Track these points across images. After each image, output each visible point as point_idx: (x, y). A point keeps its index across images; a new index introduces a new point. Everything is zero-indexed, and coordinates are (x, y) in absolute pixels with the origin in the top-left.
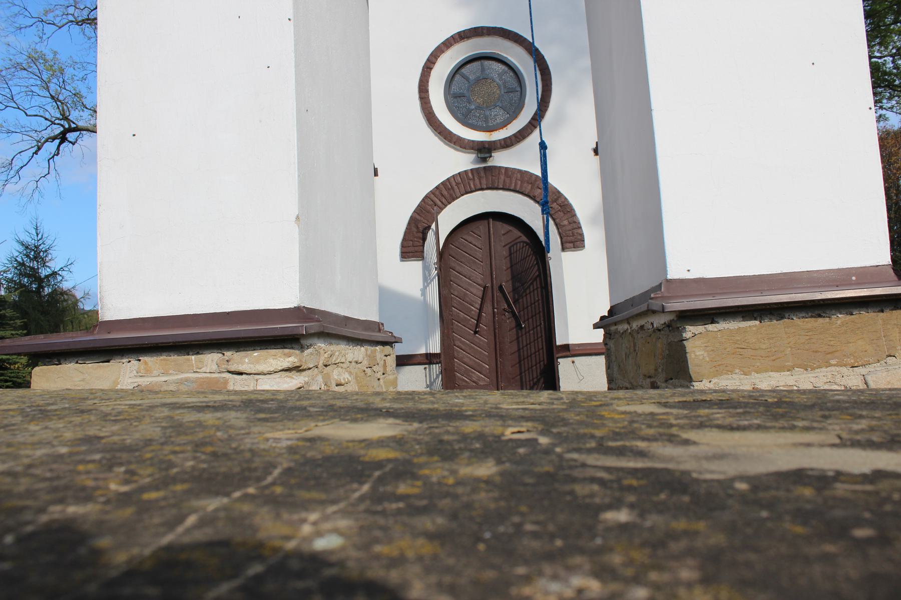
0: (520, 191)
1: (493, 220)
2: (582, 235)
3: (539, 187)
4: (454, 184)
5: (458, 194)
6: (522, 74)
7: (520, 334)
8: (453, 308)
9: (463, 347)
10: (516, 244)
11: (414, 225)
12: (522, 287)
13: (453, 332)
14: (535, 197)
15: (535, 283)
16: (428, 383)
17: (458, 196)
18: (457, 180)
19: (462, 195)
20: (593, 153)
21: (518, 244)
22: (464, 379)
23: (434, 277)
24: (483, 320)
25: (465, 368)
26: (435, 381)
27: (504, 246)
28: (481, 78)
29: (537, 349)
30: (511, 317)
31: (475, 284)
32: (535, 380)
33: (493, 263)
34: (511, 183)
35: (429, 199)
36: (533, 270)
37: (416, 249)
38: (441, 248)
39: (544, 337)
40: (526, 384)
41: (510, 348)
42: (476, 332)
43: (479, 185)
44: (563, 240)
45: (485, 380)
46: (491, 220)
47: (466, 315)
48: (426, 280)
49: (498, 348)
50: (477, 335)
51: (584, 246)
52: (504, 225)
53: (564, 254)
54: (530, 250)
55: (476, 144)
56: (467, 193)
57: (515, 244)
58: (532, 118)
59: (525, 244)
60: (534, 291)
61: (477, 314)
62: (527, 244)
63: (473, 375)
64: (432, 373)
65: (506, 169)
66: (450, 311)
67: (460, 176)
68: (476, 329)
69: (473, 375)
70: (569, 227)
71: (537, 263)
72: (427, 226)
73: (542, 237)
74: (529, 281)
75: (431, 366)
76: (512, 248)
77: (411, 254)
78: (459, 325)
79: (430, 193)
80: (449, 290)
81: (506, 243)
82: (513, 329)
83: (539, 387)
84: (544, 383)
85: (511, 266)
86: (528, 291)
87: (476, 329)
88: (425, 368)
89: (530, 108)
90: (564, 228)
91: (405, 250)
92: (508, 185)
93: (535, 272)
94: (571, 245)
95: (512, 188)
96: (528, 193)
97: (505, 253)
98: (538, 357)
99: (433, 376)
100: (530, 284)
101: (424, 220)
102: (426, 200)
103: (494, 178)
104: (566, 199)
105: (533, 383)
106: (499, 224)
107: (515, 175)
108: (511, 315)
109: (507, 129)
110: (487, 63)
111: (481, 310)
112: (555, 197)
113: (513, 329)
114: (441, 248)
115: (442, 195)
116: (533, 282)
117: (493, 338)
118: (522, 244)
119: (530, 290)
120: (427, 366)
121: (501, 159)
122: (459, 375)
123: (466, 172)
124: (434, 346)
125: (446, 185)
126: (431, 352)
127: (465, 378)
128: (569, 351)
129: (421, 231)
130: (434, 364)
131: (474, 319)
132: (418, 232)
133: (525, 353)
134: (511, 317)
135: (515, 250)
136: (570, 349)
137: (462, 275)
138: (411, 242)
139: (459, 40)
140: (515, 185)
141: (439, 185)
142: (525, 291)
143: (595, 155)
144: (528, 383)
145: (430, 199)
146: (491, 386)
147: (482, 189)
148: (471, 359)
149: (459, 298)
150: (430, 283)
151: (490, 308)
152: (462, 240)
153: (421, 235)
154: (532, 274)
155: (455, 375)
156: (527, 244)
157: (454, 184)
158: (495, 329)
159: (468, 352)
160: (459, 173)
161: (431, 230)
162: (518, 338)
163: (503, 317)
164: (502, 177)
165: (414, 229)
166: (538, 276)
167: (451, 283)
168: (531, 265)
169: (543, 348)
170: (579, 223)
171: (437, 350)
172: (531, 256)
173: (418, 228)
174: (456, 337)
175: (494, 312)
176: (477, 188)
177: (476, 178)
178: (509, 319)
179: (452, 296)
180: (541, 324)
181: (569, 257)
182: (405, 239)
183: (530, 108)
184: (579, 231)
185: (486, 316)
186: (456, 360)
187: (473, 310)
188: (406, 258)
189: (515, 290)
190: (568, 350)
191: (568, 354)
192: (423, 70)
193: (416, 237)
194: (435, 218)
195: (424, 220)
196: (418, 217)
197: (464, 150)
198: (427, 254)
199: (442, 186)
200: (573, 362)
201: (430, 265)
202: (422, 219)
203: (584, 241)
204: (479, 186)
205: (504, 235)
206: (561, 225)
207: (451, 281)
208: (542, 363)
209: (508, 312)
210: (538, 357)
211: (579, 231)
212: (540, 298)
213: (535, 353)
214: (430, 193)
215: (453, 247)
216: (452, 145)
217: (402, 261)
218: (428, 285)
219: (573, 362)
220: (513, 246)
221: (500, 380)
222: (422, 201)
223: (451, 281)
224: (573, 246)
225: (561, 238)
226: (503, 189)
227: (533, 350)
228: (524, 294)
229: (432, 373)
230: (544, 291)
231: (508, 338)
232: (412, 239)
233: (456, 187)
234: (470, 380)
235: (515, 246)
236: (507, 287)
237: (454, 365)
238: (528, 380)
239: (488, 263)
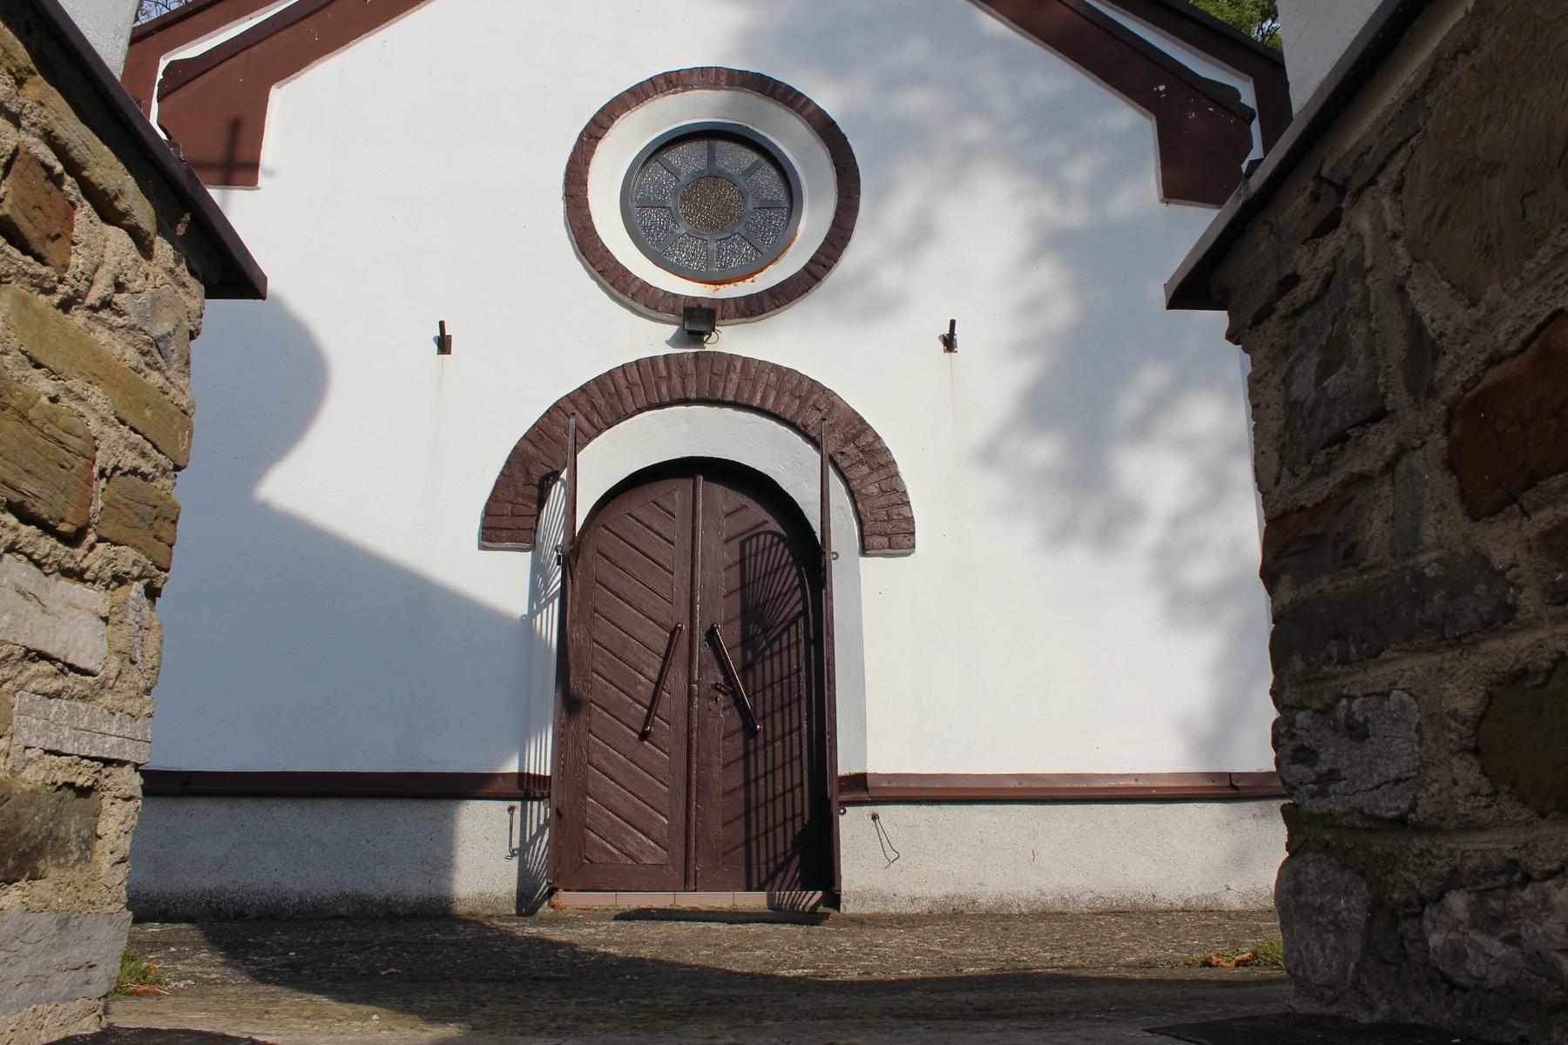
0: (772, 411)
1: (704, 480)
2: (910, 520)
3: (817, 405)
4: (622, 383)
5: (631, 408)
6: (796, 172)
7: (752, 747)
8: (595, 675)
9: (610, 770)
10: (757, 535)
11: (519, 466)
12: (762, 636)
13: (590, 731)
14: (806, 427)
15: (793, 628)
16: (516, 845)
17: (629, 411)
18: (632, 377)
19: (640, 411)
20: (941, 346)
21: (762, 537)
22: (606, 848)
23: (554, 597)
24: (663, 708)
25: (612, 820)
26: (534, 839)
27: (727, 541)
28: (706, 174)
29: (788, 786)
30: (730, 707)
31: (651, 623)
32: (779, 861)
33: (698, 576)
34: (753, 393)
35: (561, 413)
36: (788, 601)
37: (519, 522)
38: (577, 532)
39: (805, 758)
40: (759, 869)
41: (723, 778)
42: (644, 736)
43: (681, 392)
44: (865, 528)
45: (656, 854)
46: (702, 478)
47: (623, 691)
48: (536, 595)
49: (694, 778)
50: (646, 743)
51: (914, 546)
52: (731, 492)
53: (863, 560)
54: (787, 552)
55: (681, 303)
56: (651, 407)
57: (753, 536)
58: (811, 260)
59: (776, 540)
60: (789, 647)
61: (650, 694)
62: (782, 539)
63: (628, 839)
64: (528, 823)
65: (745, 360)
66: (587, 681)
67: (638, 370)
68: (646, 725)
69: (628, 839)
70: (883, 501)
71: (801, 585)
72: (550, 471)
73: (816, 525)
74: (778, 626)
75: (529, 803)
76: (748, 544)
77: (505, 534)
78: (606, 715)
79: (567, 399)
80: (589, 633)
81: (731, 534)
82: (734, 733)
83: (786, 884)
84: (800, 867)
85: (743, 586)
86: (776, 647)
87: (646, 725)
88: (511, 809)
89: (812, 227)
90: (869, 503)
91: (495, 522)
92: (746, 396)
93: (793, 605)
94: (884, 540)
95: (756, 402)
96: (791, 417)
97: (730, 555)
98: (789, 804)
99: (531, 829)
100: (782, 632)
101: (544, 459)
102: (555, 415)
103: (716, 378)
104: (877, 437)
105: (776, 867)
106: (719, 490)
107: (765, 377)
108: (730, 701)
109: (753, 281)
110: (722, 146)
111: (659, 683)
112: (853, 431)
113: (734, 733)
114: (577, 532)
115: (594, 406)
116: (782, 632)
117: (684, 753)
118: (769, 537)
119: (781, 642)
120: (518, 804)
121: (730, 340)
122: (594, 836)
123: (653, 360)
124: (539, 759)
125: (605, 385)
126: (532, 772)
127: (609, 846)
128: (866, 789)
129: (537, 483)
130: (535, 799)
131: (642, 704)
132: (528, 484)
133: (778, 723)
134: (730, 707)
135: (754, 550)
136: (869, 785)
137: (622, 599)
138: (510, 506)
139: (665, 87)
140: (764, 398)
141: (587, 384)
142: (769, 645)
143: (945, 352)
144: (763, 867)
145: (564, 412)
146: (671, 868)
147: (686, 401)
148: (626, 799)
149: (611, 652)
150: (546, 605)
151: (683, 681)
152: (630, 518)
153: (535, 492)
154: (788, 609)
155: (584, 837)
156: (782, 539)
157: (622, 383)
158: (689, 731)
159: (622, 781)
160: (637, 362)
161: (559, 483)
162: (746, 756)
163: (712, 703)
164: (735, 377)
165: (521, 478)
166: (799, 615)
167: (596, 615)
168: (785, 589)
169: (802, 784)
170: (905, 492)
171: (546, 770)
172: (788, 568)
173: (528, 474)
174: (596, 744)
175: (690, 690)
176: (676, 397)
177: (674, 375)
178: (724, 709)
179: (595, 645)
180: (800, 727)
181: (875, 570)
182: (494, 498)
183: (812, 227)
184: (904, 511)
185: (672, 700)
186: (590, 800)
187: (640, 682)
188: (491, 541)
189: (747, 641)
190: (862, 789)
191: (865, 796)
192: (580, 139)
193: (523, 496)
194: (569, 458)
195: (544, 459)
196: (531, 450)
197: (653, 314)
198: (544, 537)
199: (594, 387)
200: (875, 817)
201: (549, 563)
202: (541, 454)
203: (913, 533)
204: (679, 394)
205: (727, 515)
206: (863, 494)
207: (596, 611)
208: (798, 820)
209: (725, 694)
210: (789, 804)
211: (904, 511)
212: (803, 665)
213: (784, 794)
214: (567, 399)
215: (607, 532)
216: (628, 300)
217: (482, 547)
218: (540, 611)
219: (875, 817)
220: (750, 539)
221: (692, 855)
222: (544, 415)
223: (596, 611)
224: (886, 545)
225: (861, 523)
226: (736, 405)
227: (779, 789)
228: (768, 653)
229: (528, 823)
230: (812, 647)
231: (719, 756)
232: (511, 497)
233: (626, 392)
234: (620, 850)
235: (754, 540)
236: (729, 636)
237: (585, 811)
238: (763, 858)
239: (687, 574)
